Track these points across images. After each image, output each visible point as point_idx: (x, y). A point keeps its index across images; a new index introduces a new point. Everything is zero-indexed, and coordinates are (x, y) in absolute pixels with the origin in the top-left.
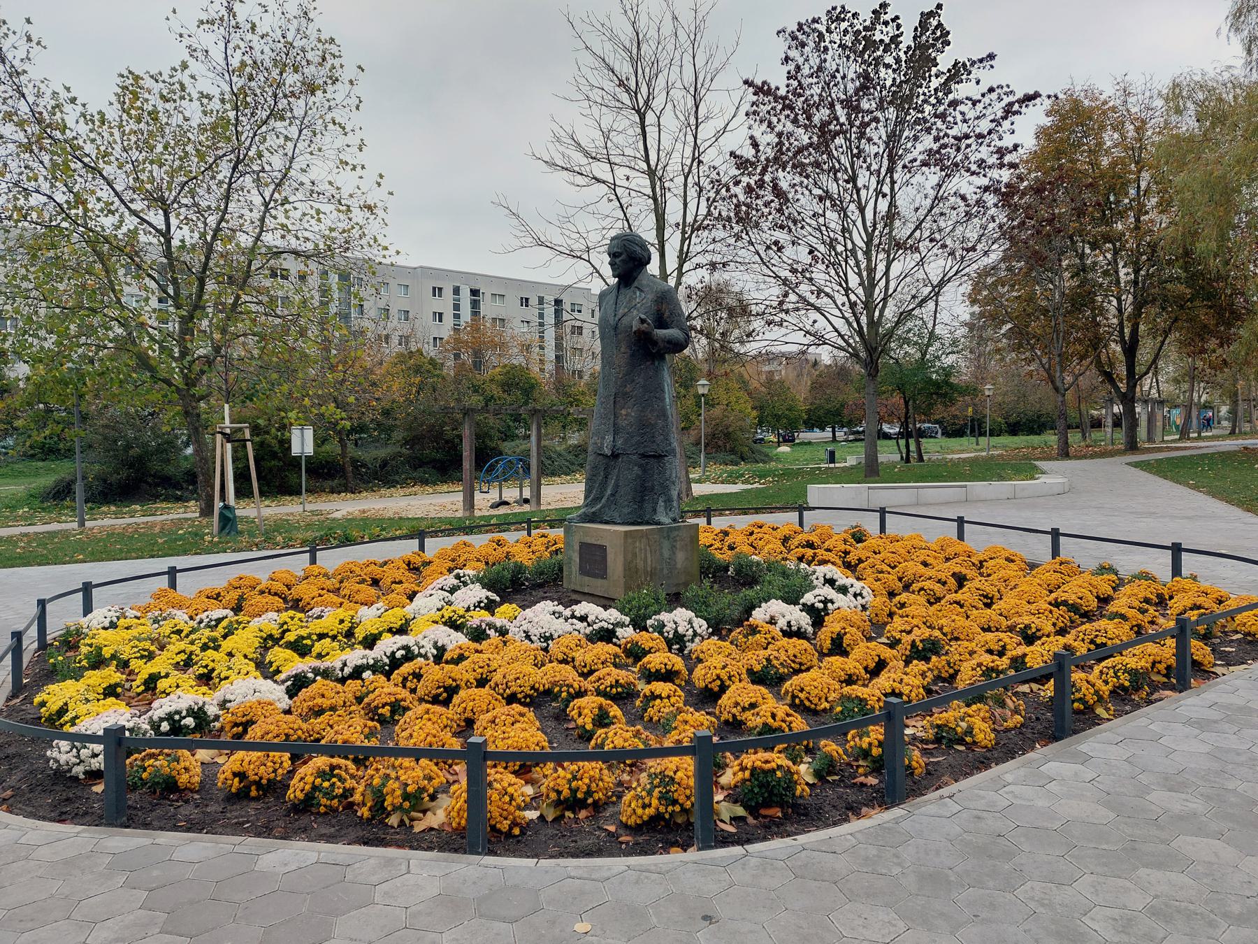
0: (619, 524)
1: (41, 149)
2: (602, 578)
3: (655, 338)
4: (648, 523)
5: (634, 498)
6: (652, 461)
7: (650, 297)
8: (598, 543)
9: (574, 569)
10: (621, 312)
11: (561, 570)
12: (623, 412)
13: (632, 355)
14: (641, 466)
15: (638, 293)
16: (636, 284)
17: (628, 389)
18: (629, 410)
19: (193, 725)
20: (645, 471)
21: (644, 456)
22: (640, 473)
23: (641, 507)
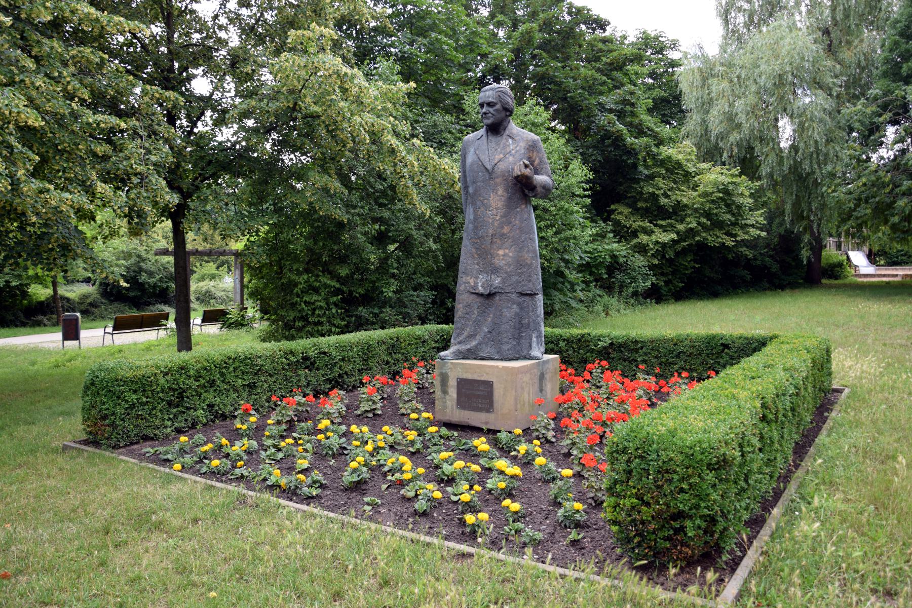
0: (497, 359)
1: (47, 435)
2: (488, 411)
3: (535, 183)
4: (525, 358)
5: (513, 335)
6: (527, 298)
7: (522, 144)
8: (482, 379)
9: (449, 403)
10: (497, 157)
11: (828, 351)
12: (501, 252)
13: (510, 198)
14: (519, 304)
15: (510, 141)
16: (507, 132)
17: (506, 230)
18: (507, 251)
19: (9, 24)
20: (522, 309)
21: (522, 294)
22: (518, 310)
23: (519, 344)
